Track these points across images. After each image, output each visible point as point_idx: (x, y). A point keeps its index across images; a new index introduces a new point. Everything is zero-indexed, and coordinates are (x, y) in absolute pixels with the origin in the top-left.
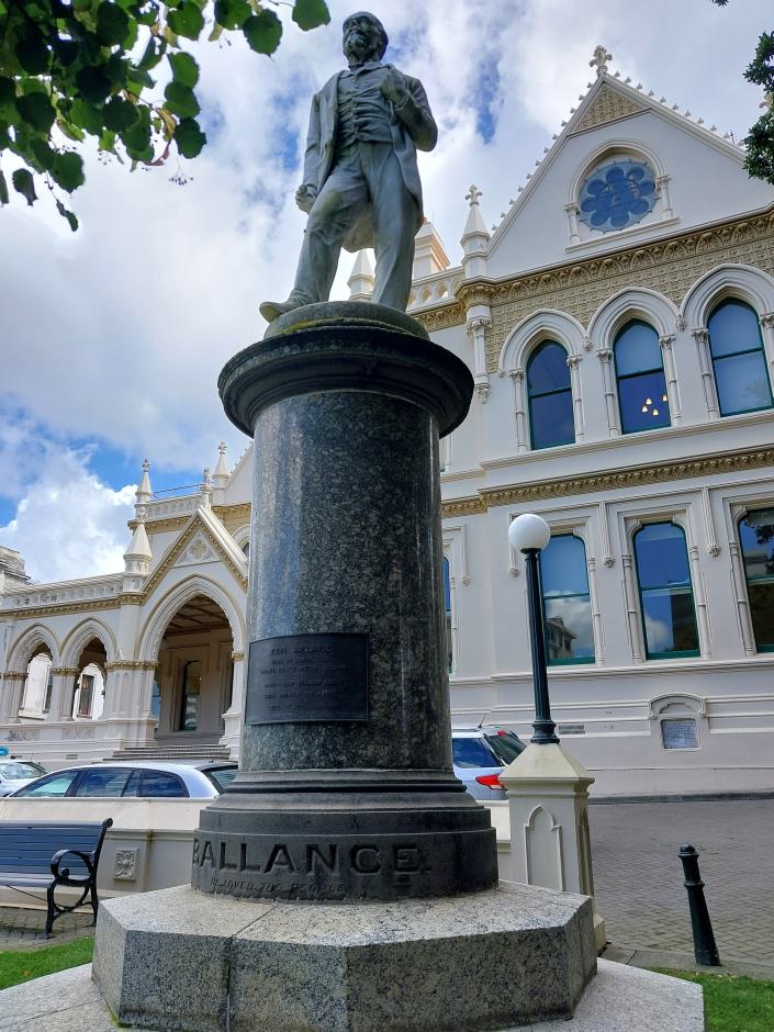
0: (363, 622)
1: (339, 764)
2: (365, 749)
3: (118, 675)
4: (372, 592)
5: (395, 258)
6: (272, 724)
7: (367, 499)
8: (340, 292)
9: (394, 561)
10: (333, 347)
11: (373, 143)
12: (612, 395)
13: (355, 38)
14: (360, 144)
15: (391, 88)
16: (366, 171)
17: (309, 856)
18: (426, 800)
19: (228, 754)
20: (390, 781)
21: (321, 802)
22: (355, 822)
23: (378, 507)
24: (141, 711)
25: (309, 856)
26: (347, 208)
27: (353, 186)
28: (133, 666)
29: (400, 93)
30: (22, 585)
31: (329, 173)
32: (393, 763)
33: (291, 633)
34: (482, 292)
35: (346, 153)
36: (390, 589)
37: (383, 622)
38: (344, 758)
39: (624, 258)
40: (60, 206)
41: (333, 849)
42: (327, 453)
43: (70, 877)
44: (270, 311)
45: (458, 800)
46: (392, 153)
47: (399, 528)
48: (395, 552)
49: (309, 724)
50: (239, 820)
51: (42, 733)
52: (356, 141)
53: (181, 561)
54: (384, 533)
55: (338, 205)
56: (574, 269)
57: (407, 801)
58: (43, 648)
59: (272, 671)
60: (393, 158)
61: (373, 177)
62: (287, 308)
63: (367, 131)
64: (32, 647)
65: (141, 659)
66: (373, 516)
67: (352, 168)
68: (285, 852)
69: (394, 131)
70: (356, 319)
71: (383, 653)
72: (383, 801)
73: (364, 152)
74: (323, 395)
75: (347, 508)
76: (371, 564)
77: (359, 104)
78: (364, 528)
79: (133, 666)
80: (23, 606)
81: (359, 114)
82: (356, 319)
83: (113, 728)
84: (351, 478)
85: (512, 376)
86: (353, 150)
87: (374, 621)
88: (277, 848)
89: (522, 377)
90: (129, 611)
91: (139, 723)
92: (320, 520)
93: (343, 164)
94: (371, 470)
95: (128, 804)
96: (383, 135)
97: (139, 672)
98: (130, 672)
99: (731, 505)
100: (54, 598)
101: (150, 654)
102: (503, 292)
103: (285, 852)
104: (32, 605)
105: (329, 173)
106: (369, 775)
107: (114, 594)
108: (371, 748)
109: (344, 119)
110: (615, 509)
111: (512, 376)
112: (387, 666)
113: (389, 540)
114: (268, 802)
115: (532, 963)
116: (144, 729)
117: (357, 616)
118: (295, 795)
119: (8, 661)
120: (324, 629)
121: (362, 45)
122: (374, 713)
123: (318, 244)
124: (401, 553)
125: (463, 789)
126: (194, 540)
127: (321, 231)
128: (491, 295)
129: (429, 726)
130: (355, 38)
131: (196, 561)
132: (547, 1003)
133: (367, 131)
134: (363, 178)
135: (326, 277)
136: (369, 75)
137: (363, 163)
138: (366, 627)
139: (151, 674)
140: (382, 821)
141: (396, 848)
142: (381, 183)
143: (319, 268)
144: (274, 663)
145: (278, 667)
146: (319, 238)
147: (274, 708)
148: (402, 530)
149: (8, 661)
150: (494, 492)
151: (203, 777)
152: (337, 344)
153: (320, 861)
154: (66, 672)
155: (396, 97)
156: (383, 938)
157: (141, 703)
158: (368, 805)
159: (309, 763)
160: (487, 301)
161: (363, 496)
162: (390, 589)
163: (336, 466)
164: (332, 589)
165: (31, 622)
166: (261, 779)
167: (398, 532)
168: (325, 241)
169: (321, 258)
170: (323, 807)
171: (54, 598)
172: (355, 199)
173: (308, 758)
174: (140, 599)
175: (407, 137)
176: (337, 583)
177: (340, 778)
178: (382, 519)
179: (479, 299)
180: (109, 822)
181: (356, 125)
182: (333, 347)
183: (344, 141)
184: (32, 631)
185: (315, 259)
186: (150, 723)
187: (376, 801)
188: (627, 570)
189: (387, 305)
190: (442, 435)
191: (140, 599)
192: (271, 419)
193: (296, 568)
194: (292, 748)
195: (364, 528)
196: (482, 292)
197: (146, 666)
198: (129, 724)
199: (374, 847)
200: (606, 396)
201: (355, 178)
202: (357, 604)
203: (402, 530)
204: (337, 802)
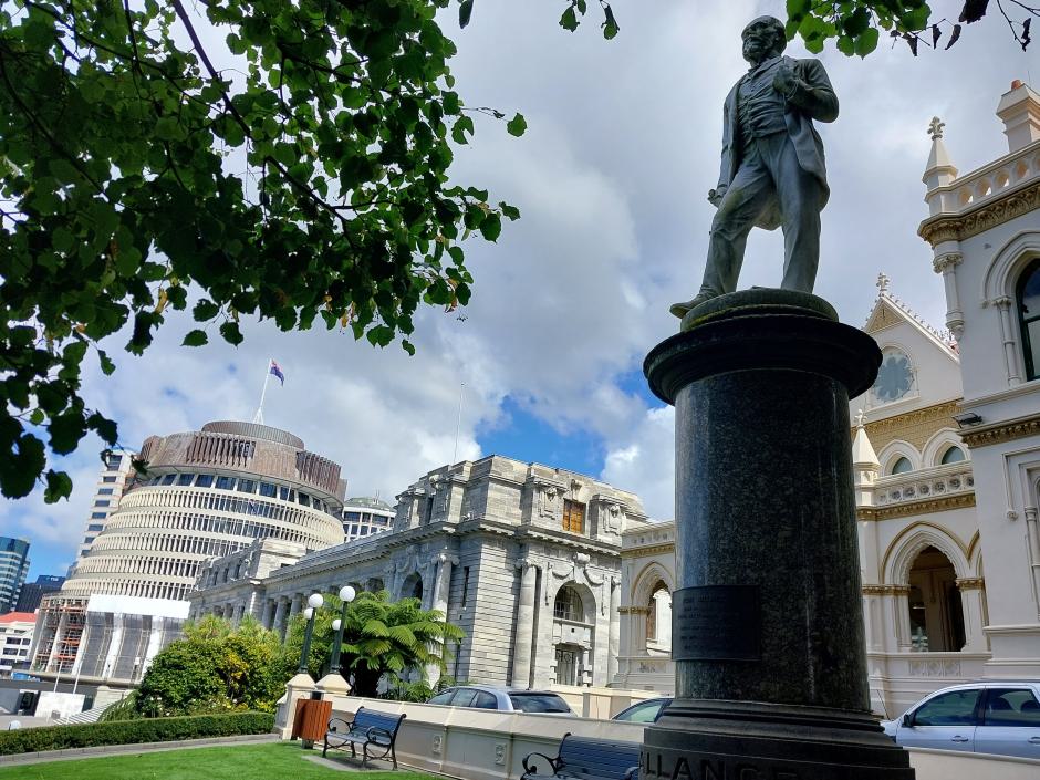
0: (754, 575)
1: (735, 696)
2: (758, 685)
4: (762, 548)
5: (796, 235)
6: (688, 661)
8: (744, 283)
9: (783, 520)
10: (679, 348)
11: (769, 136)
12: (1013, 344)
13: (751, 45)
14: (758, 141)
15: (782, 82)
16: (767, 162)
17: (703, 769)
20: (780, 714)
21: (716, 726)
22: (739, 744)
25: (703, 769)
26: (748, 202)
27: (755, 179)
29: (790, 84)
30: (641, 524)
31: (735, 171)
33: (695, 585)
34: (947, 228)
35: (747, 151)
36: (779, 545)
38: (739, 691)
39: (997, 208)
40: (950, 44)
41: (721, 764)
42: (718, 428)
44: (679, 310)
45: (875, 738)
46: (788, 140)
47: (787, 489)
48: (785, 510)
49: (712, 661)
52: (754, 139)
55: (737, 203)
56: (979, 215)
57: (793, 732)
58: (661, 585)
59: (685, 617)
60: (789, 145)
61: (773, 164)
62: (693, 304)
63: (762, 128)
64: (652, 584)
66: (761, 481)
67: (753, 163)
68: (686, 765)
69: (788, 119)
70: (742, 307)
72: (769, 730)
73: (763, 146)
74: (715, 378)
75: (737, 475)
77: (754, 106)
78: (752, 491)
80: (640, 545)
81: (754, 114)
82: (742, 307)
84: (740, 448)
85: (997, 304)
86: (752, 147)
87: (764, 575)
88: (681, 760)
89: (1008, 304)
92: (715, 487)
93: (746, 161)
94: (758, 439)
96: (779, 126)
97: (889, 599)
98: (878, 598)
99: (1029, 471)
100: (665, 537)
101: (901, 580)
102: (970, 224)
103: (686, 765)
104: (647, 544)
105: (735, 171)
106: (761, 706)
108: (763, 684)
109: (743, 121)
110: (1015, 462)
111: (997, 304)
117: (748, 571)
118: (699, 720)
119: (632, 597)
120: (720, 582)
121: (757, 50)
122: (765, 655)
123: (721, 243)
124: (791, 511)
127: (722, 230)
128: (957, 229)
129: (823, 669)
130: (751, 45)
133: (762, 128)
134: (764, 169)
135: (730, 269)
136: (763, 76)
137: (763, 155)
138: (756, 580)
139: (904, 601)
140: (763, 746)
142: (780, 169)
143: (726, 257)
144: (685, 610)
145: (689, 613)
146: (722, 237)
147: (686, 648)
150: (1003, 427)
151: (508, 699)
152: (717, 337)
153: (712, 774)
155: (787, 89)
156: (25, 727)
158: (754, 732)
159: (712, 694)
160: (954, 235)
161: (751, 463)
162: (779, 545)
163: (727, 439)
164: (726, 547)
165: (651, 559)
166: (702, 706)
167: (787, 493)
168: (726, 237)
169: (724, 254)
170: (717, 730)
171: (665, 537)
172: (756, 191)
173: (712, 690)
175: (802, 120)
176: (730, 541)
177: (735, 708)
179: (947, 235)
180: (404, 716)
181: (751, 125)
182: (714, 339)
183: (744, 141)
184: (650, 568)
185: (719, 256)
187: (761, 729)
188: (1032, 524)
189: (790, 288)
190: (850, 399)
192: (684, 396)
193: (702, 527)
194: (701, 681)
195: (752, 491)
196: (947, 228)
197: (897, 592)
199: (755, 767)
201: (756, 171)
202: (748, 560)
203: (792, 490)
204: (730, 727)
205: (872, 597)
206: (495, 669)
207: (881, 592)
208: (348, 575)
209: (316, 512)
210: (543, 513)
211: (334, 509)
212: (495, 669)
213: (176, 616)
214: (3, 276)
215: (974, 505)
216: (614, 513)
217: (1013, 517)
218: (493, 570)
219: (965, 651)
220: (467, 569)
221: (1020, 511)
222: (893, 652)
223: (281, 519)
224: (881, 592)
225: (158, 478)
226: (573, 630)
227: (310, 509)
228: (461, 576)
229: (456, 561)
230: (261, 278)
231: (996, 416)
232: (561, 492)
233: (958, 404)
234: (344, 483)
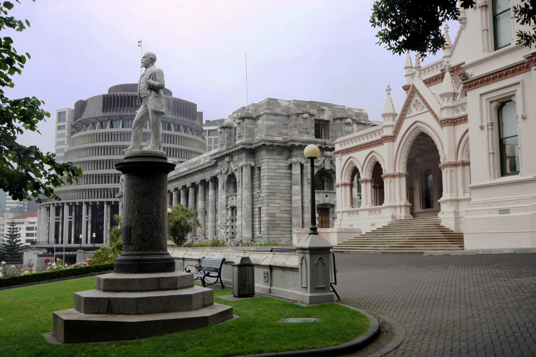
3: (447, 171)
7: (131, 198)
18: (155, 257)
19: (440, 222)
23: (133, 199)
24: (401, 199)
28: (456, 165)
32: (135, 250)
37: (133, 224)
43: (210, 275)
50: (126, 260)
51: (360, 213)
53: (410, 113)
54: (133, 205)
65: (460, 159)
71: (133, 230)
76: (131, 212)
79: (456, 165)
83: (388, 209)
90: (386, 145)
91: (401, 206)
95: (263, 254)
97: (397, 179)
98: (392, 179)
107: (378, 137)
110: (485, 97)
112: (134, 232)
113: (135, 206)
114: (122, 257)
115: (133, 283)
116: (403, 209)
119: (341, 177)
125: (169, 254)
126: (414, 100)
131: (417, 113)
132: (135, 289)
141: (127, 265)
148: (138, 203)
149: (341, 177)
154: (345, 185)
157: (346, 202)
165: (368, 151)
174: (392, 138)
178: (133, 202)
186: (406, 206)
188: (490, 131)
191: (392, 138)
197: (400, 175)
198: (395, 207)
200: (483, 30)
205: (390, 179)
206: (281, 222)
207: (394, 176)
208: (210, 174)
209: (186, 135)
210: (301, 130)
211: (197, 131)
212: (281, 222)
213: (348, 105)
214: (1, 188)
215: (468, 122)
216: (348, 124)
217: (482, 128)
218: (274, 167)
219: (384, 205)
220: (259, 168)
221: (485, 124)
222: (461, 197)
223: (105, 183)
224: (394, 176)
225: (88, 125)
226: (327, 196)
227: (182, 134)
228: (257, 172)
229: (253, 164)
230: (54, 155)
231: (475, 73)
232: (312, 115)
233: (462, 66)
234: (201, 114)
